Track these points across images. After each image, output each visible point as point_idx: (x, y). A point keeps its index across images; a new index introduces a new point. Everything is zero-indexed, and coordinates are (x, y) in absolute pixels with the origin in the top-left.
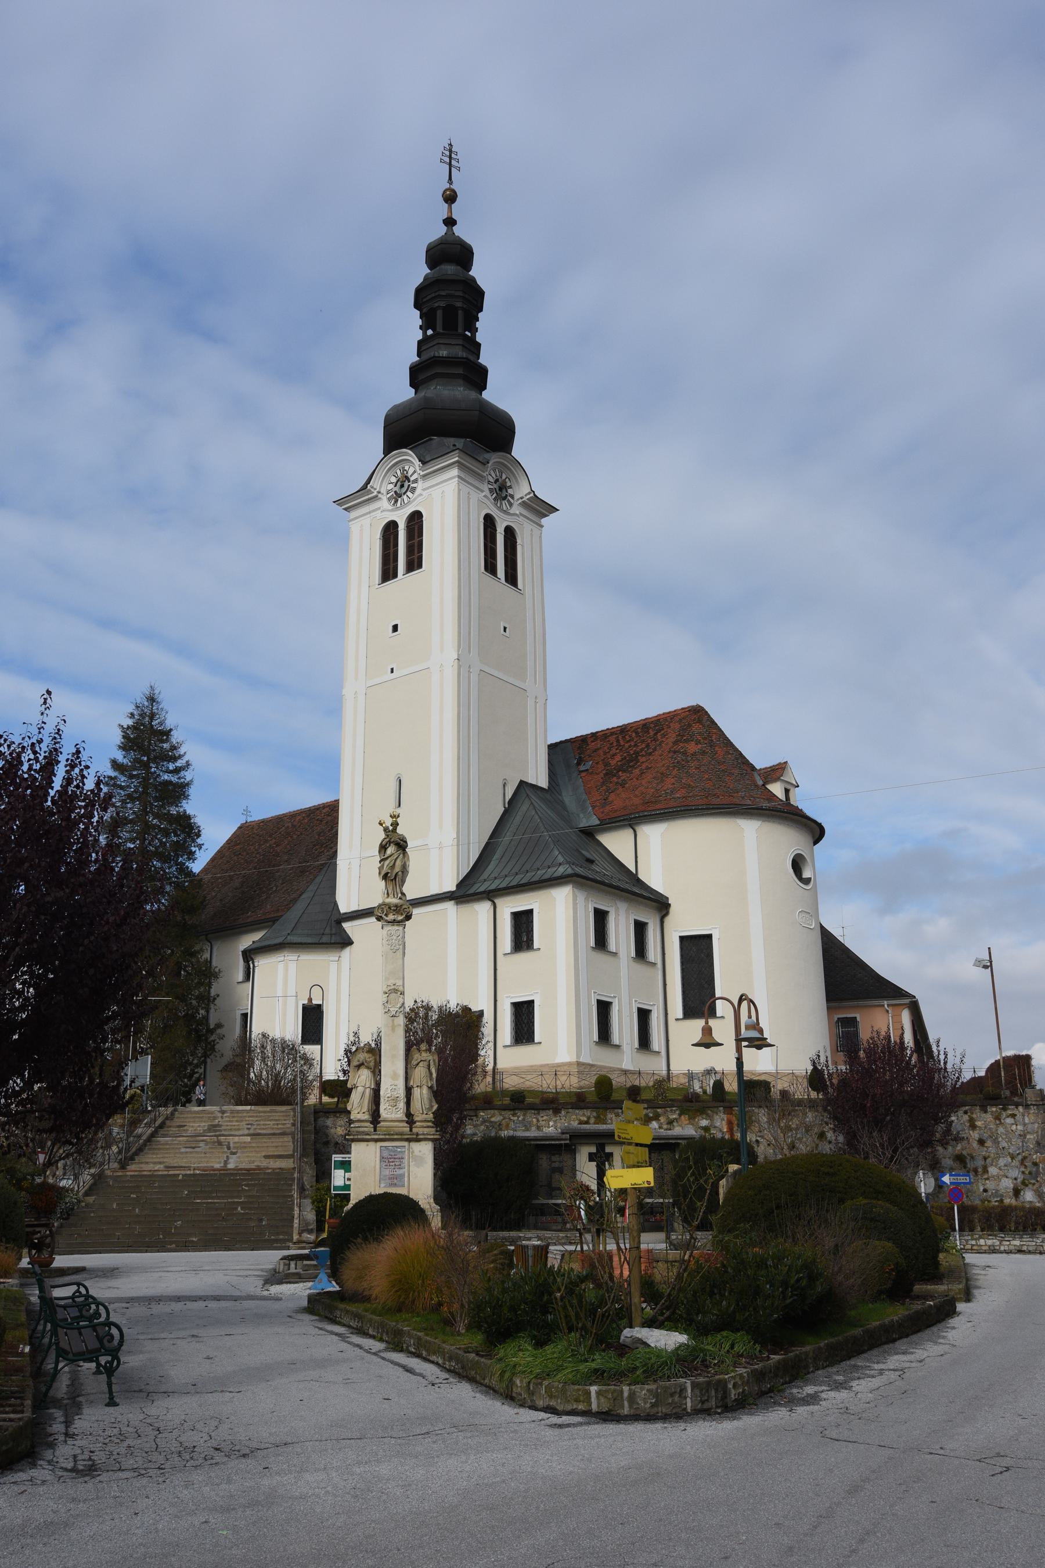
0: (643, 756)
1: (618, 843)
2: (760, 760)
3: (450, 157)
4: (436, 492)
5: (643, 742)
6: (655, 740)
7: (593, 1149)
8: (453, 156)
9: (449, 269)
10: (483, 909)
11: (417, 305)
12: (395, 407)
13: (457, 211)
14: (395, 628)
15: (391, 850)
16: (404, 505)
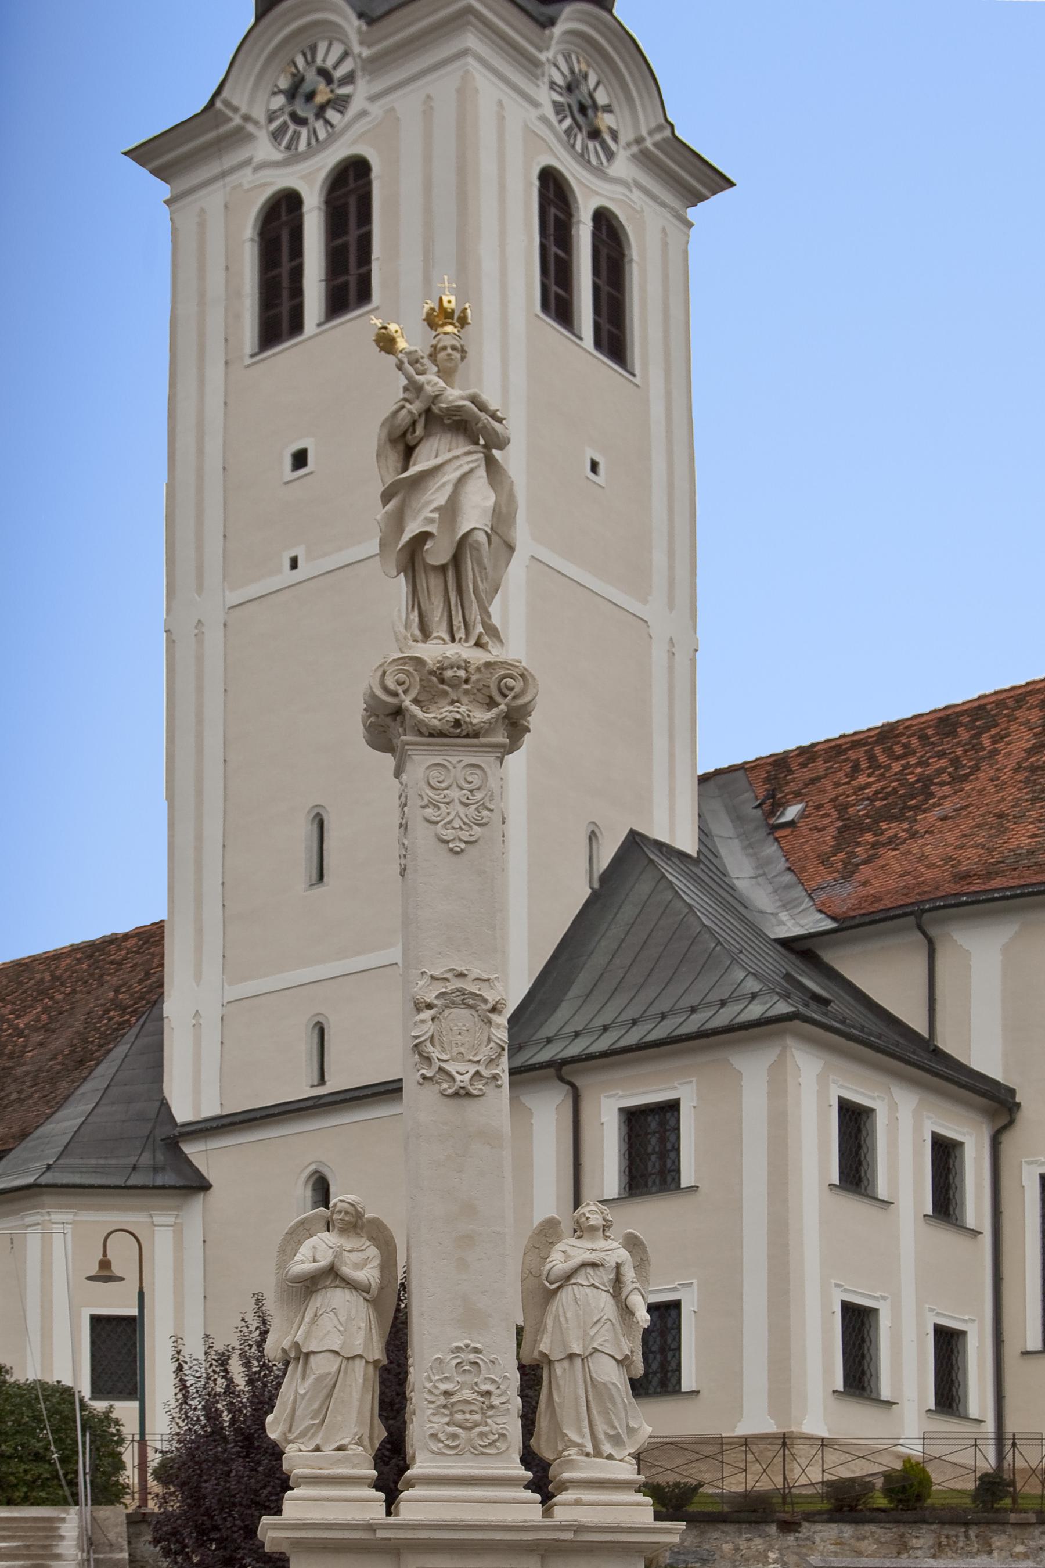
0: (942, 784)
4: (407, 104)
5: (941, 755)
6: (977, 747)
14: (300, 459)
16: (316, 146)
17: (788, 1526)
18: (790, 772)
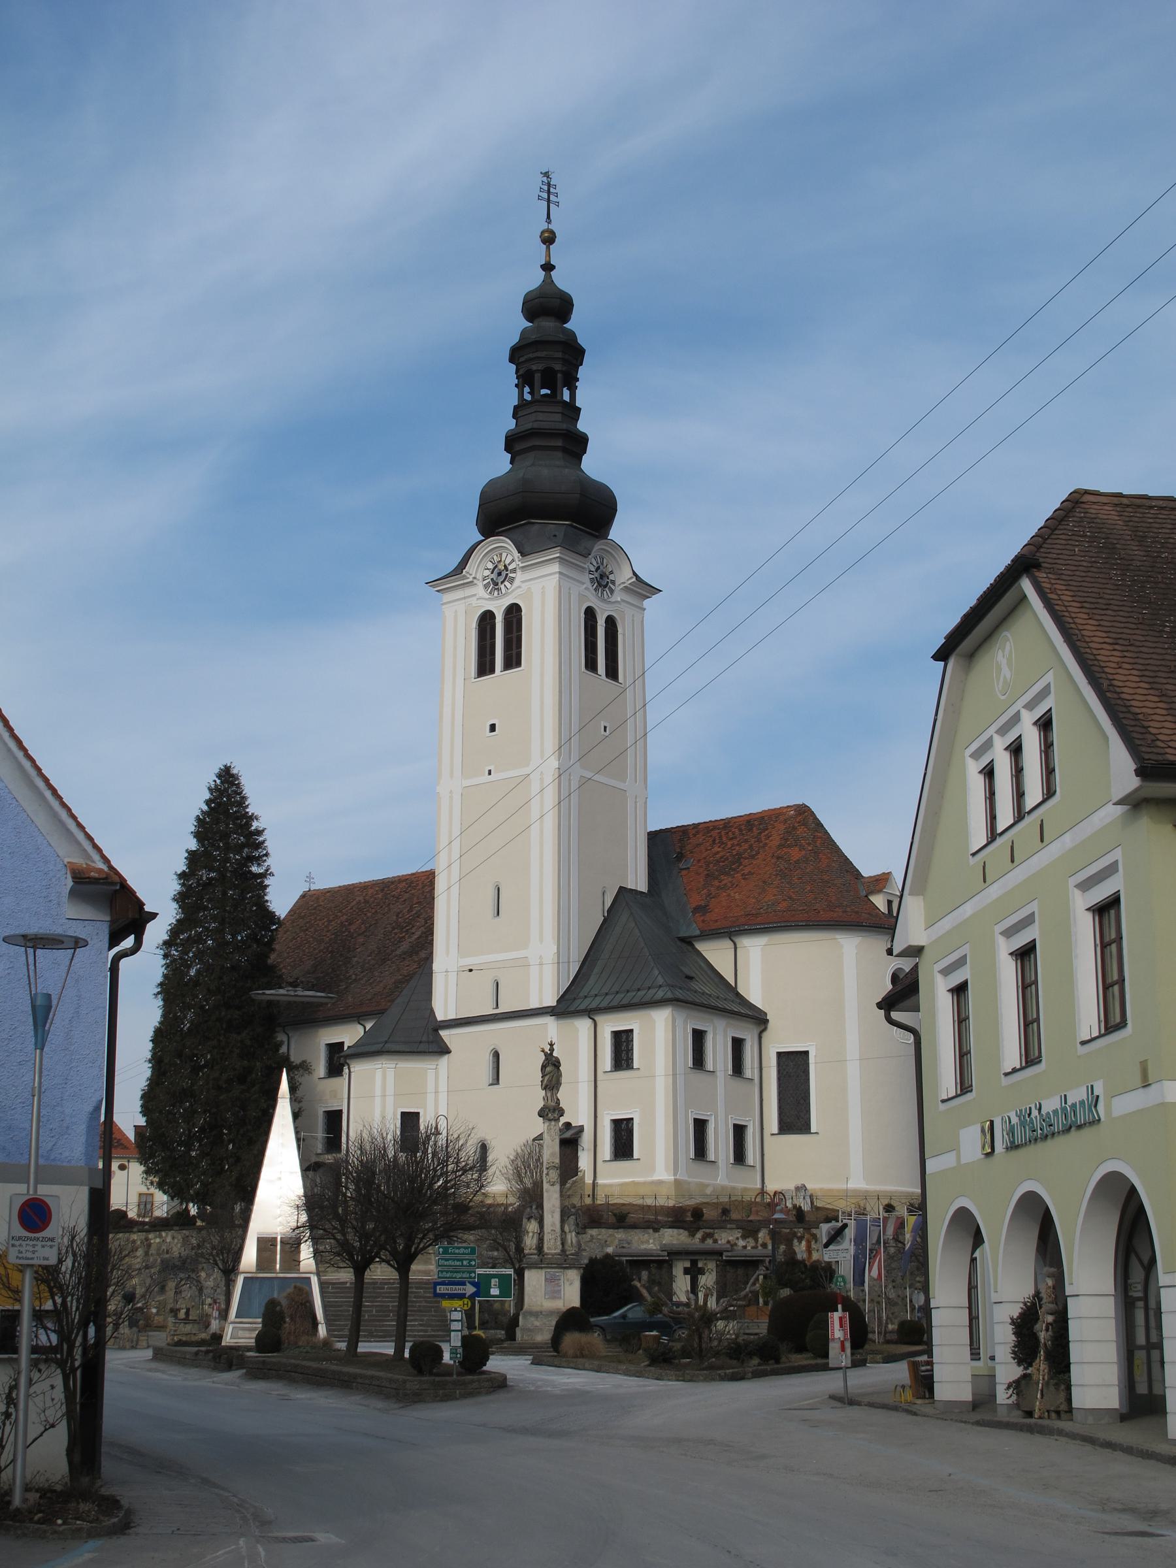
1: (717, 954)
2: (868, 870)
3: (549, 192)
5: (746, 841)
6: (759, 841)
7: (688, 1264)
8: (552, 190)
9: (548, 324)
10: (583, 1026)
11: (511, 360)
12: (492, 483)
13: (557, 255)
14: (493, 728)
15: (548, 1069)
16: (501, 596)
17: (656, 1230)
18: (689, 838)
